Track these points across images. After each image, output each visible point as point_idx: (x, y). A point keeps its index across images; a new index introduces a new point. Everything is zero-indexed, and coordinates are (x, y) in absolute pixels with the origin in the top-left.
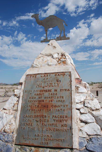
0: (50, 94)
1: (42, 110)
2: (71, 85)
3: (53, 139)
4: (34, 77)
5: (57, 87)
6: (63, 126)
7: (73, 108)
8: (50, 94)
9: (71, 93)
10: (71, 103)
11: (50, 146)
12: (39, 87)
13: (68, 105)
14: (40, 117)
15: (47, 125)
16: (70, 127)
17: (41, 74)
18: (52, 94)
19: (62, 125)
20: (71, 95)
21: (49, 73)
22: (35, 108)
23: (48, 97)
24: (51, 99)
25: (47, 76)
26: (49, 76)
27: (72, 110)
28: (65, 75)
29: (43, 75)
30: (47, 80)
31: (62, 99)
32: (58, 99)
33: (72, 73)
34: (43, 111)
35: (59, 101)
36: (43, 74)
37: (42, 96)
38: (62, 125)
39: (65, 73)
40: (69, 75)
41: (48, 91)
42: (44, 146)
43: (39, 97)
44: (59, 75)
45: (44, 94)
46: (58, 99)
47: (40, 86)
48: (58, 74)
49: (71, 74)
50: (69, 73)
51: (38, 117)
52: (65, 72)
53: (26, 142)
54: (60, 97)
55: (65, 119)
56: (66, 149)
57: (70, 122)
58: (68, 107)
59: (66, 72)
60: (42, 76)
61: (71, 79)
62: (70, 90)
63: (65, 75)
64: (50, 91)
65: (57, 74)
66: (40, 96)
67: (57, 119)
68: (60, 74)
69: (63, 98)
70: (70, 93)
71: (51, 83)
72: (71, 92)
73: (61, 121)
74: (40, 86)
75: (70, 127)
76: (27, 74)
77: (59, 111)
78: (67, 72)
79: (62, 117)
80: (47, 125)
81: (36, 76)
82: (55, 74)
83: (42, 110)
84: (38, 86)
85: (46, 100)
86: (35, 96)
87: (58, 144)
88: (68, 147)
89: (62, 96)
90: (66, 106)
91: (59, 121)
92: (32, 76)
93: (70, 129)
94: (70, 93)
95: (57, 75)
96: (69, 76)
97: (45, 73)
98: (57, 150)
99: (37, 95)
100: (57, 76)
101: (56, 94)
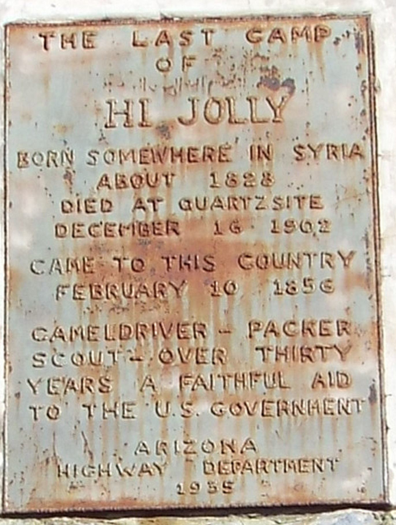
0: (221, 178)
1: (170, 291)
2: (374, 119)
3: (264, 462)
4: (78, 41)
5: (270, 127)
6: (327, 381)
7: (385, 272)
8: (221, 178)
9: (375, 175)
10: (371, 239)
11: (42, 510)
12: (128, 124)
13: (352, 253)
14: (161, 339)
15: (218, 382)
16: (372, 389)
17: (134, 21)
18: (232, 181)
19: (319, 381)
20: (375, 184)
21: (199, 21)
22: (112, 280)
23: (209, 204)
24: (234, 211)
25: (186, 37)
26: (197, 38)
27: (377, 284)
28: (326, 40)
29: (154, 33)
30: (193, 73)
31: (308, 214)
32: (284, 215)
33: (376, 22)
34: (178, 296)
35: (289, 225)
36: (152, 22)
37: (161, 193)
38: (319, 381)
39: (328, 24)
40: (359, 39)
41: (200, 154)
42: (60, 519)
43: (140, 201)
44: (277, 35)
45: (175, 181)
46: (284, 215)
47: (136, 116)
48: (275, 25)
49: (371, 37)
50: (350, 25)
51: (149, 336)
52: (324, 17)
53: (79, 496)
54: (299, 199)
55: (335, 339)
56: (350, 511)
57: (372, 365)
58: (353, 264)
59: (332, 16)
60: (140, 39)
61: (372, 74)
62: (366, 148)
63: (327, 42)
64: (216, 157)
65: (263, 25)
66: (146, 193)
67: (284, 341)
68: (287, 29)
69: (314, 204)
70: (369, 175)
71: (220, 93)
72: (375, 163)
73: (309, 357)
74: (136, 116)
75: (372, 389)
76: (12, 17)
77: (291, 291)
78: (344, 17)
79: (317, 328)
80: (218, 382)
81: (97, 41)
82: (250, 25)
83: (170, 291)
84: (119, 120)
85: (193, 224)
86: (105, 193)
87: (298, 488)
88: (357, 498)
89: (306, 192)
90: (338, 262)
91: (298, 352)
92: (58, 32)
93: (372, 399)
94: (369, 171)
95: (266, 35)
96: (357, 46)
97: (166, 19)
98: (280, 518)
99: (121, 184)
100: (264, 44)
101: (267, 178)
